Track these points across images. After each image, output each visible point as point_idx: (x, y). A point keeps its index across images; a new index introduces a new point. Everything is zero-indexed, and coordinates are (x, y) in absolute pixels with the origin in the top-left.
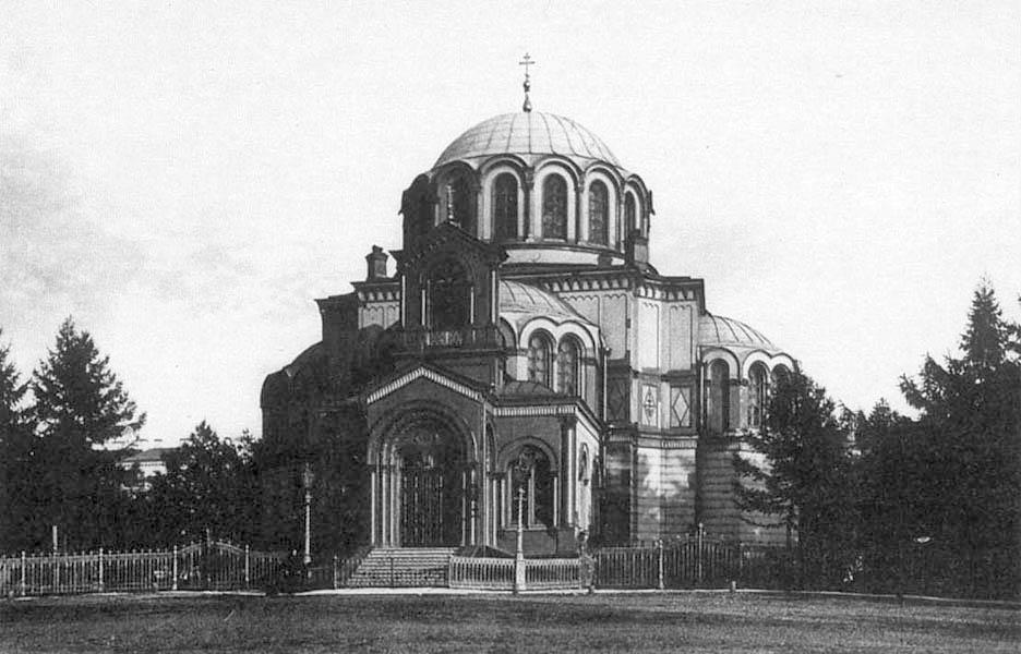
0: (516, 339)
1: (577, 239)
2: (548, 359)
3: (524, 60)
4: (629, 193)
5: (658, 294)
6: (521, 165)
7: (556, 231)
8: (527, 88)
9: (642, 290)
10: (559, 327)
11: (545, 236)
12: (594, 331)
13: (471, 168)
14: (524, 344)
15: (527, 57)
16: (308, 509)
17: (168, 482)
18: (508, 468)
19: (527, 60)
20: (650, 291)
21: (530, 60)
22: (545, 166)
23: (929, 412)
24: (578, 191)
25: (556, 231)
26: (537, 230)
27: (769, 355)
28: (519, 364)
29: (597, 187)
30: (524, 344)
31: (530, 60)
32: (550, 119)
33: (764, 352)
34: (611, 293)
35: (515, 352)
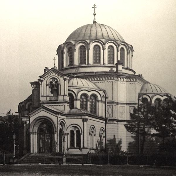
0: (76, 96)
1: (104, 64)
2: (87, 101)
3: (94, 7)
4: (122, 48)
5: (125, 80)
6: (86, 43)
7: (97, 59)
8: (95, 15)
9: (119, 79)
10: (90, 92)
11: (94, 63)
12: (101, 92)
13: (72, 44)
14: (79, 97)
15: (95, 5)
16: (25, 146)
17: (46, 132)
18: (141, 127)
19: (95, 7)
20: (122, 79)
21: (95, 6)
22: (93, 43)
23: (169, 119)
24: (104, 49)
25: (97, 59)
26: (91, 61)
27: (161, 96)
28: (77, 104)
29: (110, 48)
30: (79, 97)
31: (95, 6)
32: (100, 25)
33: (160, 95)
34: (108, 81)
35: (76, 99)
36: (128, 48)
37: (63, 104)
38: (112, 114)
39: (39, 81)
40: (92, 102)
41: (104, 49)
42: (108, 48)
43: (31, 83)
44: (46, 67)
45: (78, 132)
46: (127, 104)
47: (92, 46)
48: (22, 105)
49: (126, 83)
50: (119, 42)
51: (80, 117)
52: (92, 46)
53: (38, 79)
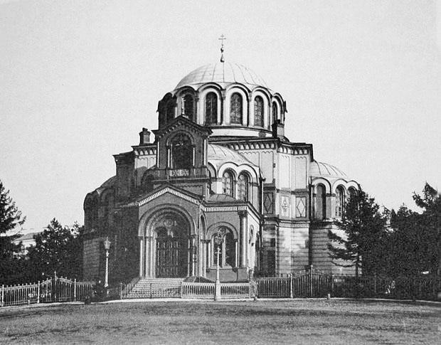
2: (233, 182)
5: (289, 151)
8: (222, 51)
11: (231, 122)
14: (220, 175)
20: (285, 150)
24: (222, 100)
36: (269, 96)
37: (200, 184)
38: (271, 209)
39: (134, 150)
40: (241, 185)
41: (222, 100)
42: (255, 100)
43: (114, 156)
44: (144, 129)
45: (230, 237)
46: (293, 193)
47: (228, 95)
48: (92, 197)
49: (290, 156)
50: (250, 87)
51: (235, 209)
52: (228, 95)
53: (132, 147)
